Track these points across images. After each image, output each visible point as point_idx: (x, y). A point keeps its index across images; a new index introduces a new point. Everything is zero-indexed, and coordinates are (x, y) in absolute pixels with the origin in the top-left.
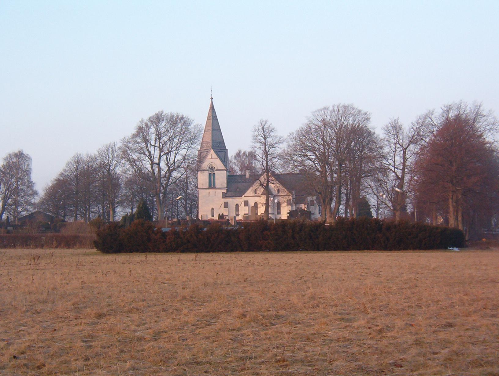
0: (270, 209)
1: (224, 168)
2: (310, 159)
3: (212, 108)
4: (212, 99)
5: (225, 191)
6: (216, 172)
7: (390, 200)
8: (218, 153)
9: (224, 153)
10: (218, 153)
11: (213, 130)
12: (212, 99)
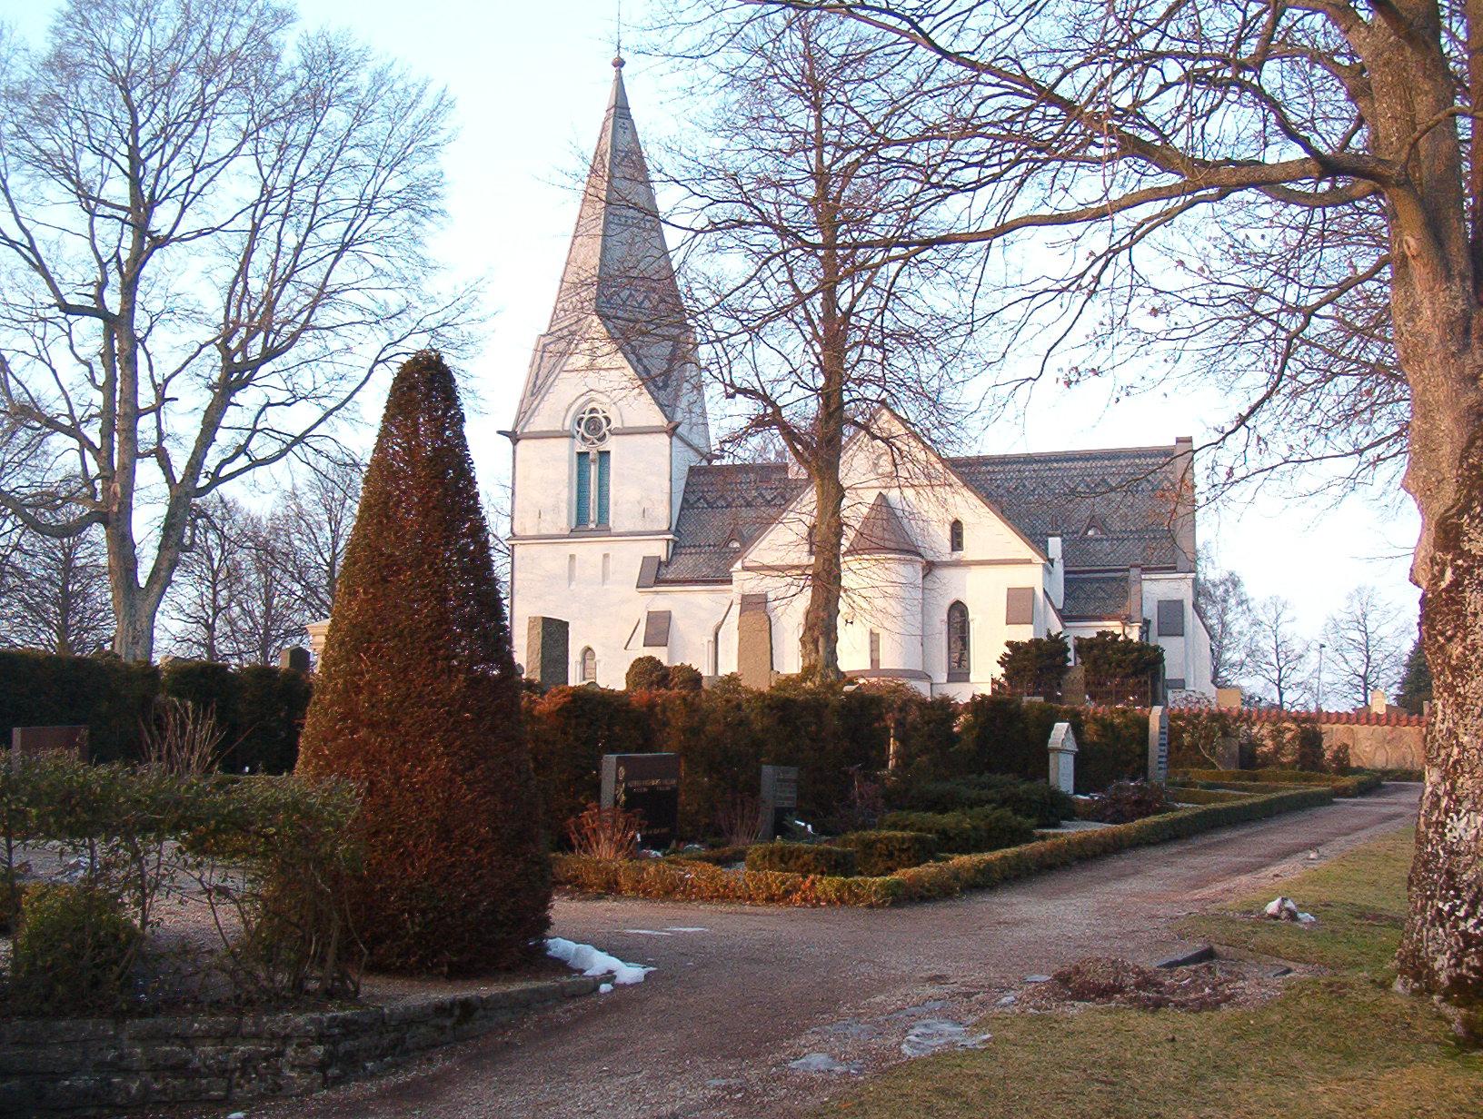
1: (658, 419)
3: (621, 110)
4: (619, 64)
5: (659, 549)
6: (611, 444)
12: (619, 64)
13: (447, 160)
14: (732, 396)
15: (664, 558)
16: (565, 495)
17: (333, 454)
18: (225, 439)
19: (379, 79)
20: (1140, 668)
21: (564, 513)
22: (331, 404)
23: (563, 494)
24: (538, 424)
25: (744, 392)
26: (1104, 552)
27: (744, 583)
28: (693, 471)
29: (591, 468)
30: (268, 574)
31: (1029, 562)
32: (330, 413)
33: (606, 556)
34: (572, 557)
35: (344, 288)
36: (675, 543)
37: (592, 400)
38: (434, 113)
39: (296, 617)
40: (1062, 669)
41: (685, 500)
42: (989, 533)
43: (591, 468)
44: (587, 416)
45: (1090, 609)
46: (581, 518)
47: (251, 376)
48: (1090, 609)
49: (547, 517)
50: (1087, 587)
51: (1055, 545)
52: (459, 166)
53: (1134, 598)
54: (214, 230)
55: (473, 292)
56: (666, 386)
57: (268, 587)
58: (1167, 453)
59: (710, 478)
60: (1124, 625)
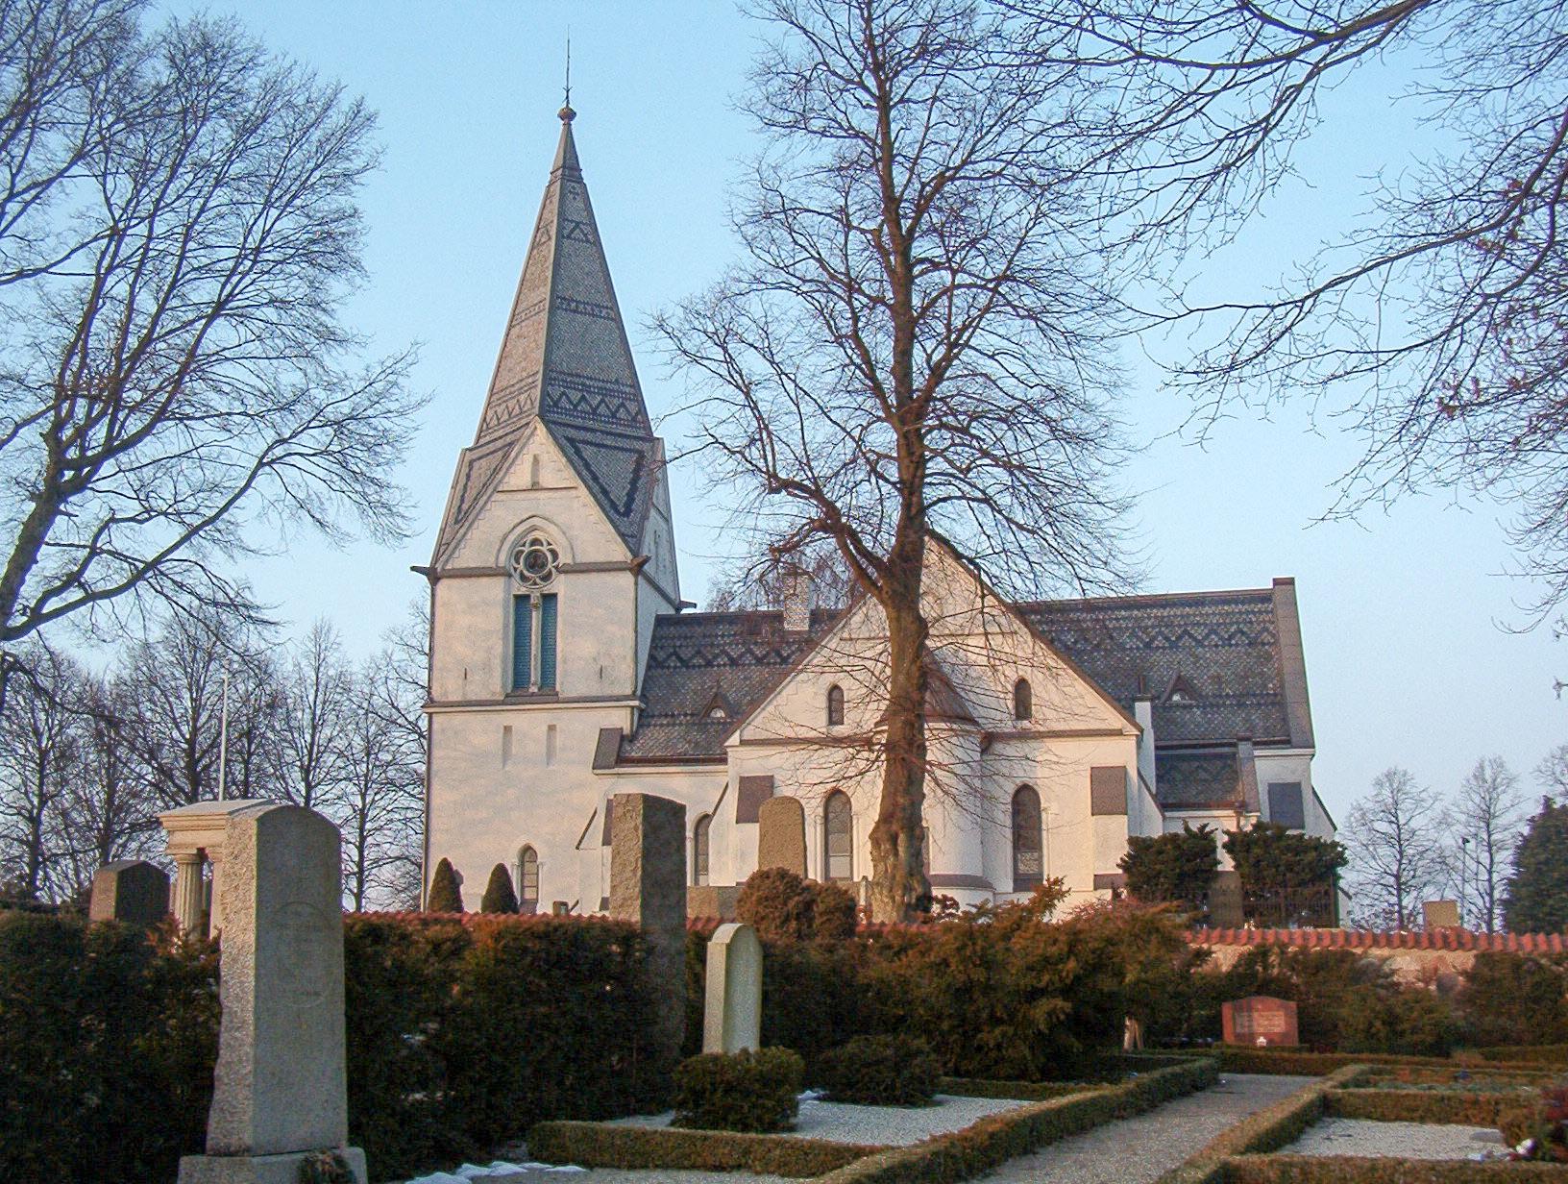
0: (935, 814)
1: (619, 552)
2: (867, 90)
3: (569, 171)
4: (568, 115)
5: (620, 719)
6: (560, 585)
7: (186, 944)
8: (588, 452)
9: (627, 463)
10: (588, 452)
11: (559, 303)
12: (568, 115)
13: (364, 196)
14: (777, 491)
15: (627, 731)
16: (499, 649)
17: (201, 590)
18: (50, 562)
19: (271, 87)
20: (1294, 867)
21: (498, 673)
22: (196, 521)
23: (497, 648)
24: (465, 558)
25: (787, 485)
26: (1196, 722)
27: (744, 760)
28: (661, 621)
29: (532, 618)
30: (110, 752)
31: (1119, 733)
32: (194, 531)
33: (552, 728)
34: (507, 729)
35: (220, 356)
36: (641, 711)
37: (534, 528)
38: (348, 131)
39: (145, 807)
40: (1208, 872)
41: (651, 657)
42: (1066, 695)
43: (532, 618)
44: (527, 549)
45: (1191, 793)
46: (520, 679)
47: (91, 474)
48: (1191, 793)
49: (476, 677)
50: (1185, 766)
51: (1143, 710)
52: (380, 203)
53: (1245, 778)
54: (37, 272)
55: (393, 370)
56: (627, 513)
57: (111, 767)
58: (1263, 597)
59: (684, 630)
60: (1239, 814)
